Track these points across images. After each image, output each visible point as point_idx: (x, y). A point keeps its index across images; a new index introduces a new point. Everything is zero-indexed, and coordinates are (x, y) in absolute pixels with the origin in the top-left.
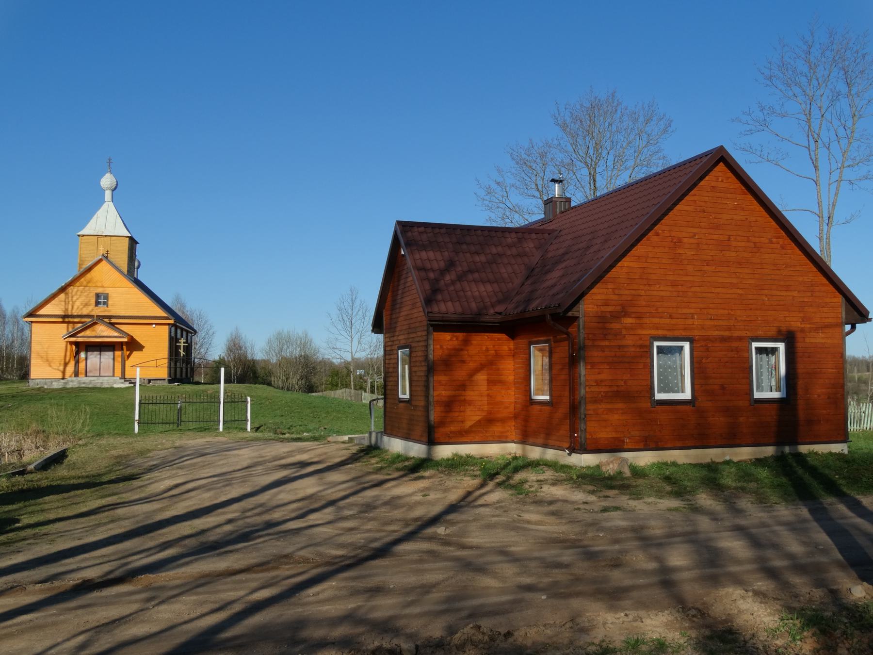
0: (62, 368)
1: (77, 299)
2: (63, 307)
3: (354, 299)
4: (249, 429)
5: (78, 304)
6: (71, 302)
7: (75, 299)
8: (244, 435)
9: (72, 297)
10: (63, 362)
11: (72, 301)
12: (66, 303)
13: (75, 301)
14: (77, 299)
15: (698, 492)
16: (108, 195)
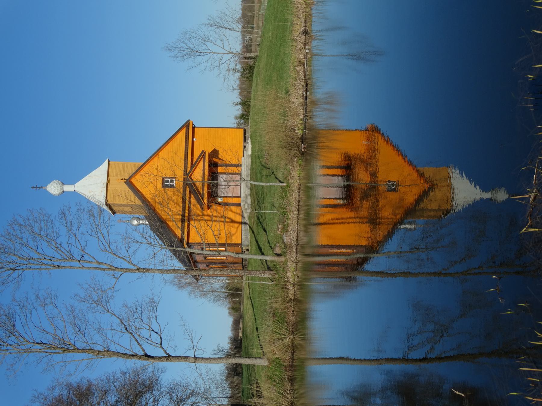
0: (236, 225)
2: (179, 222)
10: (231, 224)
16: (68, 188)
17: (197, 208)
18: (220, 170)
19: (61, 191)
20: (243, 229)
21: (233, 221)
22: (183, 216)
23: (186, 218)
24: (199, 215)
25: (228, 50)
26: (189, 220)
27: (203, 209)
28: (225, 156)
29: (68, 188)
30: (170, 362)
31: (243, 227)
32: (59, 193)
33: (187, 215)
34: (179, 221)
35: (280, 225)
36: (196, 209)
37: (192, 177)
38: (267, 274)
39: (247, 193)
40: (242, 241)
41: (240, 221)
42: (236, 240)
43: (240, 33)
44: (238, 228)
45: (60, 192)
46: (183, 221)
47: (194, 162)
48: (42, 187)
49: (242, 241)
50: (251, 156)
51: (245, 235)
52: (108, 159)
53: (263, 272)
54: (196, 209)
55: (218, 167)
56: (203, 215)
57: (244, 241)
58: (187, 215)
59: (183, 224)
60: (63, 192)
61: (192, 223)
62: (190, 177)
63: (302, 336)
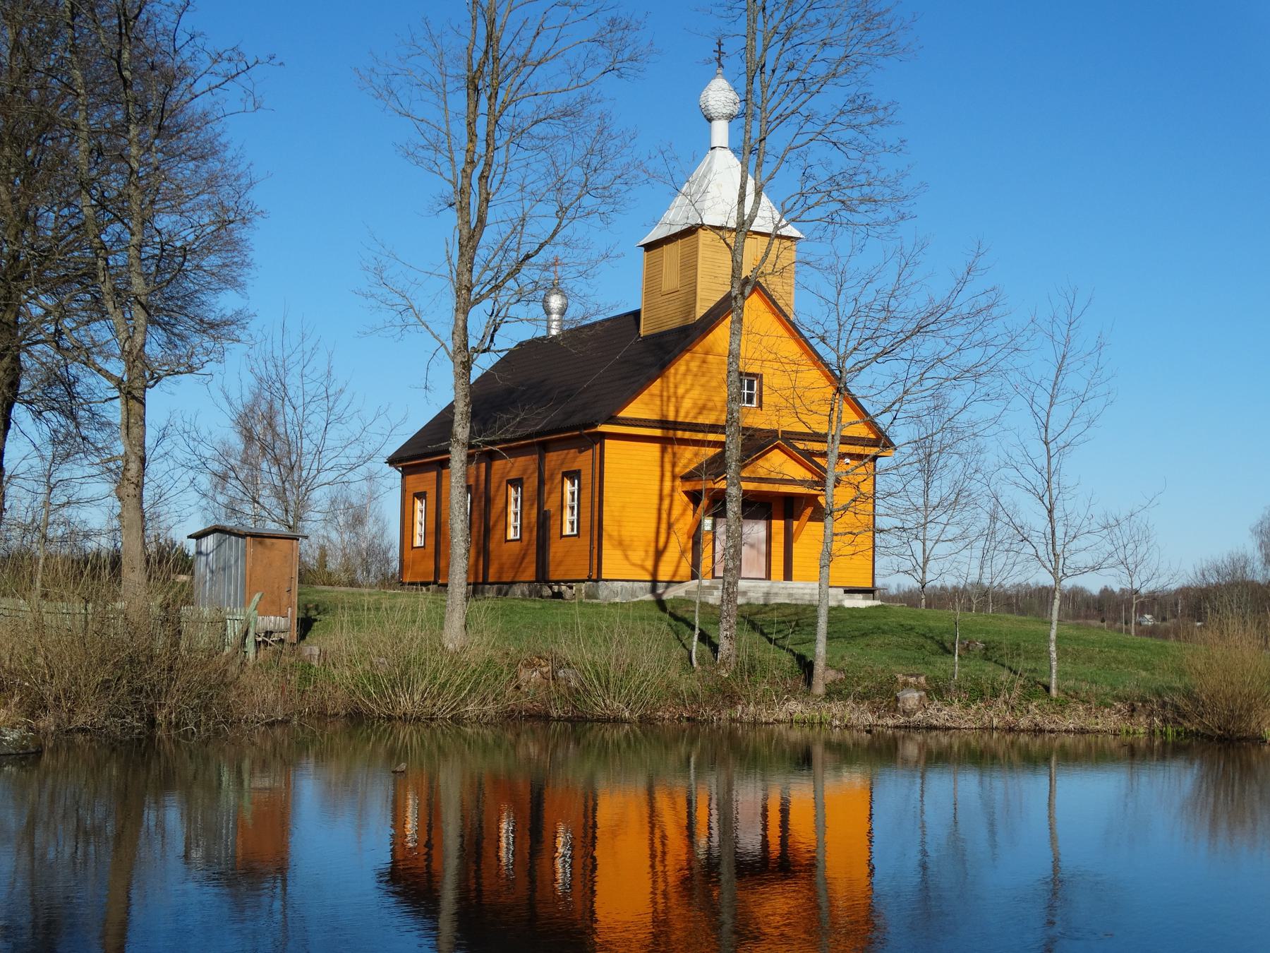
0: (649, 564)
1: (687, 391)
2: (657, 409)
3: (552, 53)
4: (1133, 634)
5: (687, 404)
6: (673, 400)
7: (681, 391)
8: (1122, 637)
9: (676, 387)
10: (652, 550)
11: (677, 398)
12: (664, 399)
13: (683, 397)
14: (687, 391)
15: (199, 105)
16: (720, 132)
17: (690, 460)
18: (778, 525)
19: (714, 114)
20: (636, 584)
21: (659, 554)
22: (676, 425)
23: (671, 433)
24: (674, 465)
25: (933, 553)
26: (664, 441)
27: (686, 478)
28: (810, 535)
29: (720, 132)
30: (456, 374)
31: (642, 584)
32: (710, 108)
33: (680, 434)
34: (663, 415)
35: (927, 679)
36: (689, 458)
37: (777, 451)
38: (731, 647)
39: (750, 594)
40: (607, 580)
41: (661, 578)
42: (613, 563)
43: (974, 577)
44: (643, 567)
45: (713, 111)
46: (663, 423)
47: (817, 459)
48: (721, 66)
49: (607, 580)
50: (839, 606)
51: (622, 590)
52: (802, 236)
53: (734, 636)
54: (689, 458)
55: (784, 519)
56: (674, 477)
57: (607, 587)
58: (680, 434)
59: (655, 424)
60: (710, 120)
61: (655, 448)
62: (777, 447)
63: (550, 747)
